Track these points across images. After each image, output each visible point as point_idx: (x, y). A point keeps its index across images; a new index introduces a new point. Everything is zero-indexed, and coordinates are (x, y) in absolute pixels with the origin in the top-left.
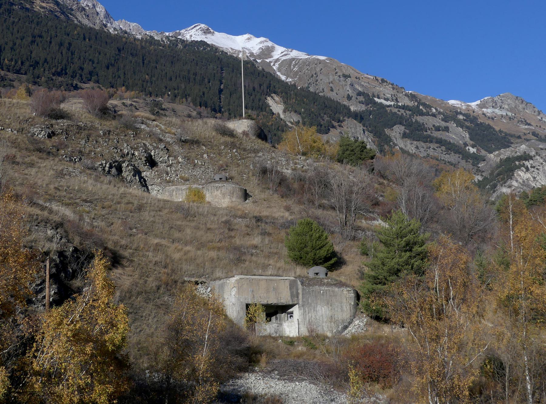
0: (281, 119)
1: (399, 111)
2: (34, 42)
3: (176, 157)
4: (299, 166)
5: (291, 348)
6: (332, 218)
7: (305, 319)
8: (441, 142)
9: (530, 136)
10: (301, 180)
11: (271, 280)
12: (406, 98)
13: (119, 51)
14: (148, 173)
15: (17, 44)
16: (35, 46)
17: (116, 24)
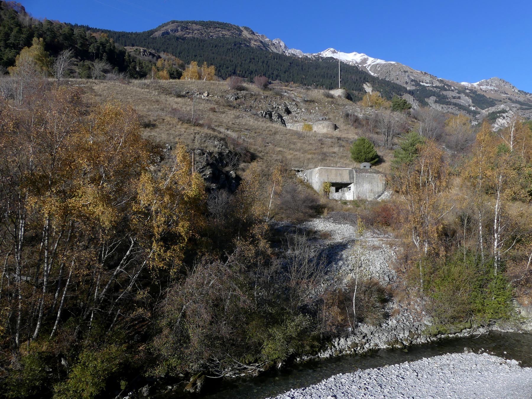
3: (301, 109)
5: (345, 206)
6: (381, 138)
7: (357, 191)
8: (455, 105)
9: (507, 100)
10: (367, 119)
12: (438, 82)
16: (251, 64)
17: (290, 51)
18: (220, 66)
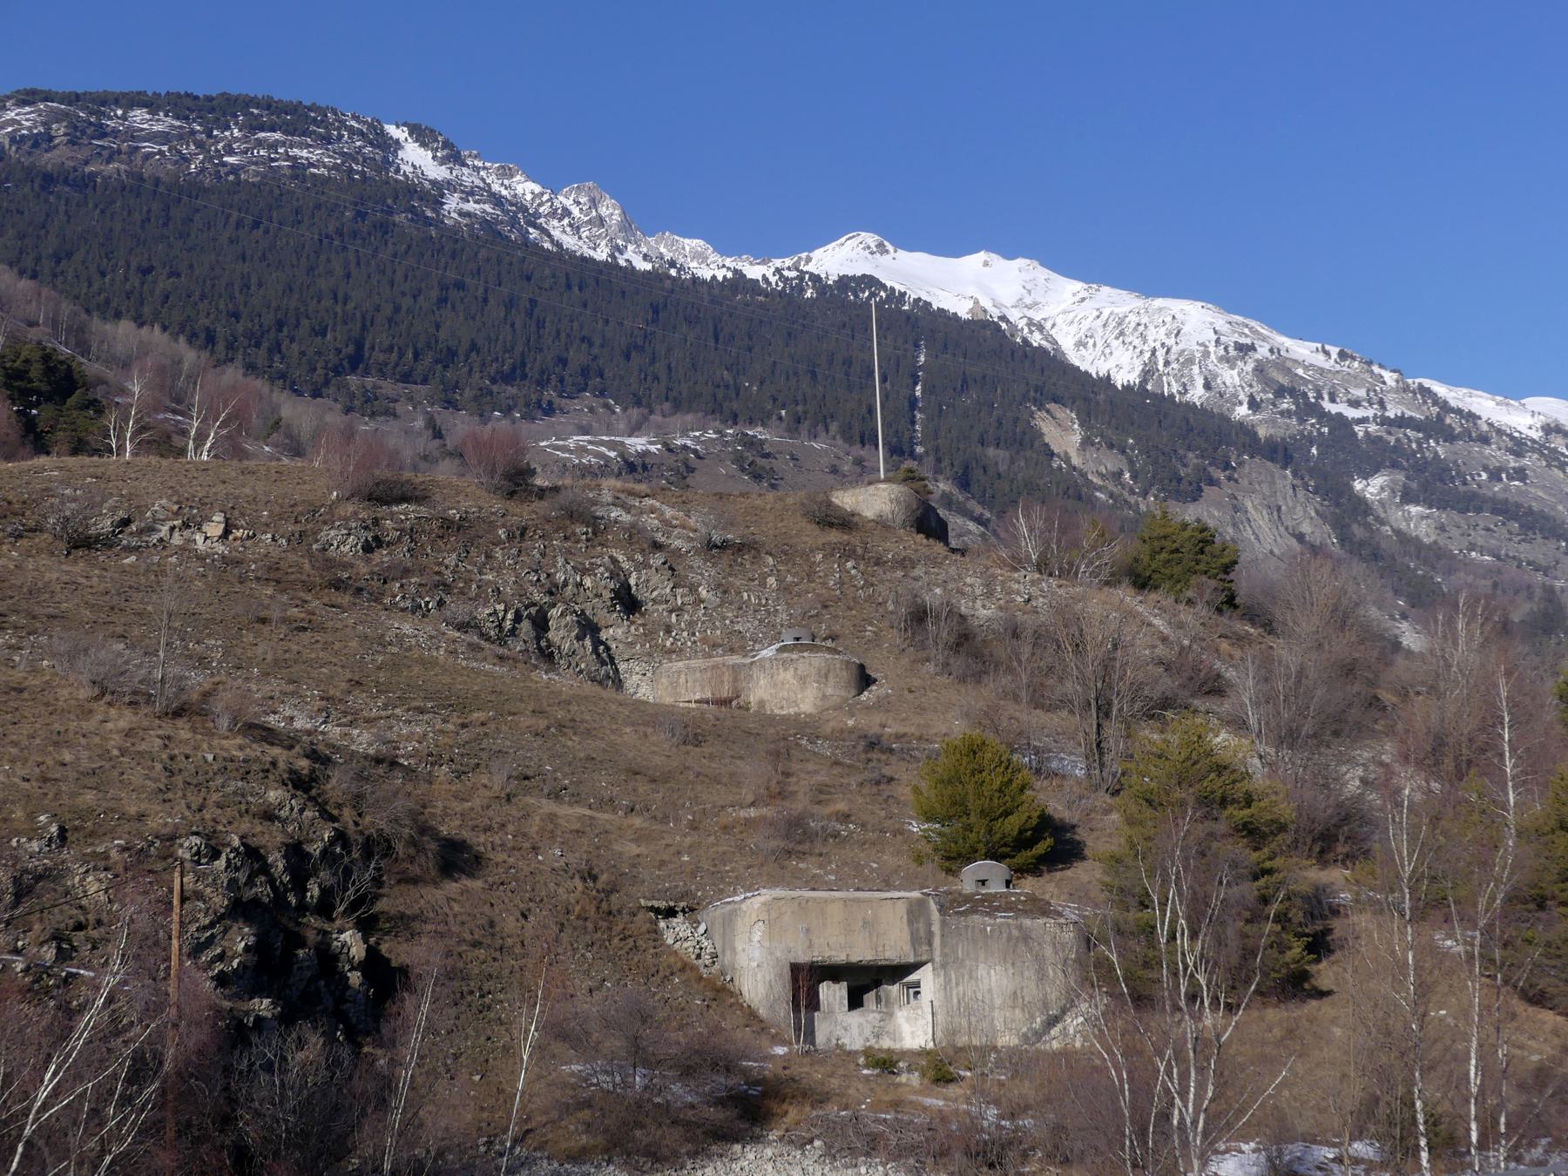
0: (1075, 468)
1: (1390, 433)
2: (446, 300)
3: (693, 589)
4: (1019, 599)
7: (948, 998)
8: (1504, 509)
11: (857, 901)
13: (656, 312)
14: (620, 631)
15: (404, 308)
18: (280, 325)
